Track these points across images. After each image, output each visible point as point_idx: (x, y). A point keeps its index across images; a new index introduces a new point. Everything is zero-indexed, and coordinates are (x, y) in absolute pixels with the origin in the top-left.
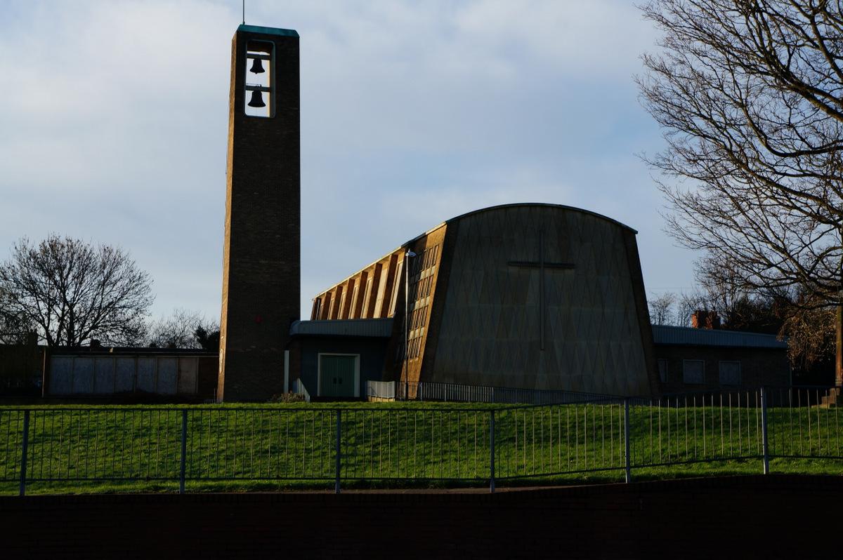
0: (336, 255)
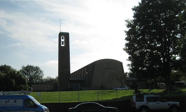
0: (75, 66)
